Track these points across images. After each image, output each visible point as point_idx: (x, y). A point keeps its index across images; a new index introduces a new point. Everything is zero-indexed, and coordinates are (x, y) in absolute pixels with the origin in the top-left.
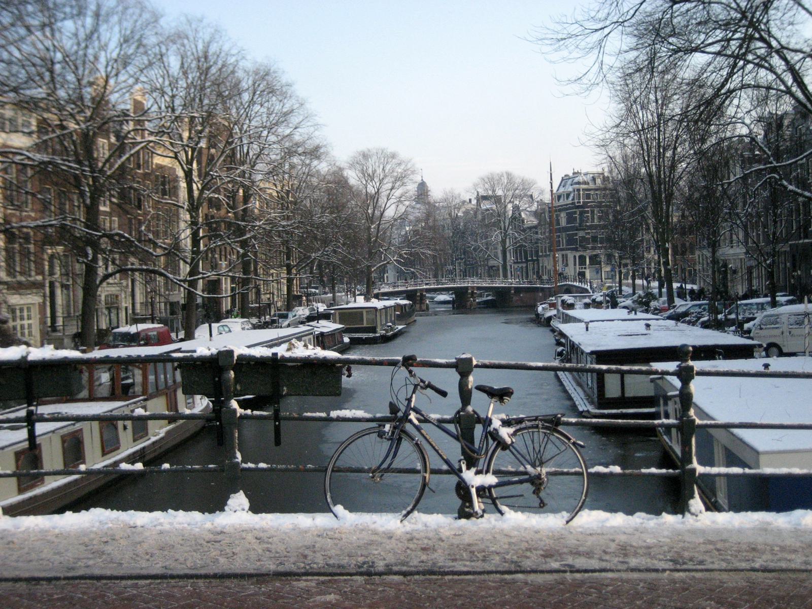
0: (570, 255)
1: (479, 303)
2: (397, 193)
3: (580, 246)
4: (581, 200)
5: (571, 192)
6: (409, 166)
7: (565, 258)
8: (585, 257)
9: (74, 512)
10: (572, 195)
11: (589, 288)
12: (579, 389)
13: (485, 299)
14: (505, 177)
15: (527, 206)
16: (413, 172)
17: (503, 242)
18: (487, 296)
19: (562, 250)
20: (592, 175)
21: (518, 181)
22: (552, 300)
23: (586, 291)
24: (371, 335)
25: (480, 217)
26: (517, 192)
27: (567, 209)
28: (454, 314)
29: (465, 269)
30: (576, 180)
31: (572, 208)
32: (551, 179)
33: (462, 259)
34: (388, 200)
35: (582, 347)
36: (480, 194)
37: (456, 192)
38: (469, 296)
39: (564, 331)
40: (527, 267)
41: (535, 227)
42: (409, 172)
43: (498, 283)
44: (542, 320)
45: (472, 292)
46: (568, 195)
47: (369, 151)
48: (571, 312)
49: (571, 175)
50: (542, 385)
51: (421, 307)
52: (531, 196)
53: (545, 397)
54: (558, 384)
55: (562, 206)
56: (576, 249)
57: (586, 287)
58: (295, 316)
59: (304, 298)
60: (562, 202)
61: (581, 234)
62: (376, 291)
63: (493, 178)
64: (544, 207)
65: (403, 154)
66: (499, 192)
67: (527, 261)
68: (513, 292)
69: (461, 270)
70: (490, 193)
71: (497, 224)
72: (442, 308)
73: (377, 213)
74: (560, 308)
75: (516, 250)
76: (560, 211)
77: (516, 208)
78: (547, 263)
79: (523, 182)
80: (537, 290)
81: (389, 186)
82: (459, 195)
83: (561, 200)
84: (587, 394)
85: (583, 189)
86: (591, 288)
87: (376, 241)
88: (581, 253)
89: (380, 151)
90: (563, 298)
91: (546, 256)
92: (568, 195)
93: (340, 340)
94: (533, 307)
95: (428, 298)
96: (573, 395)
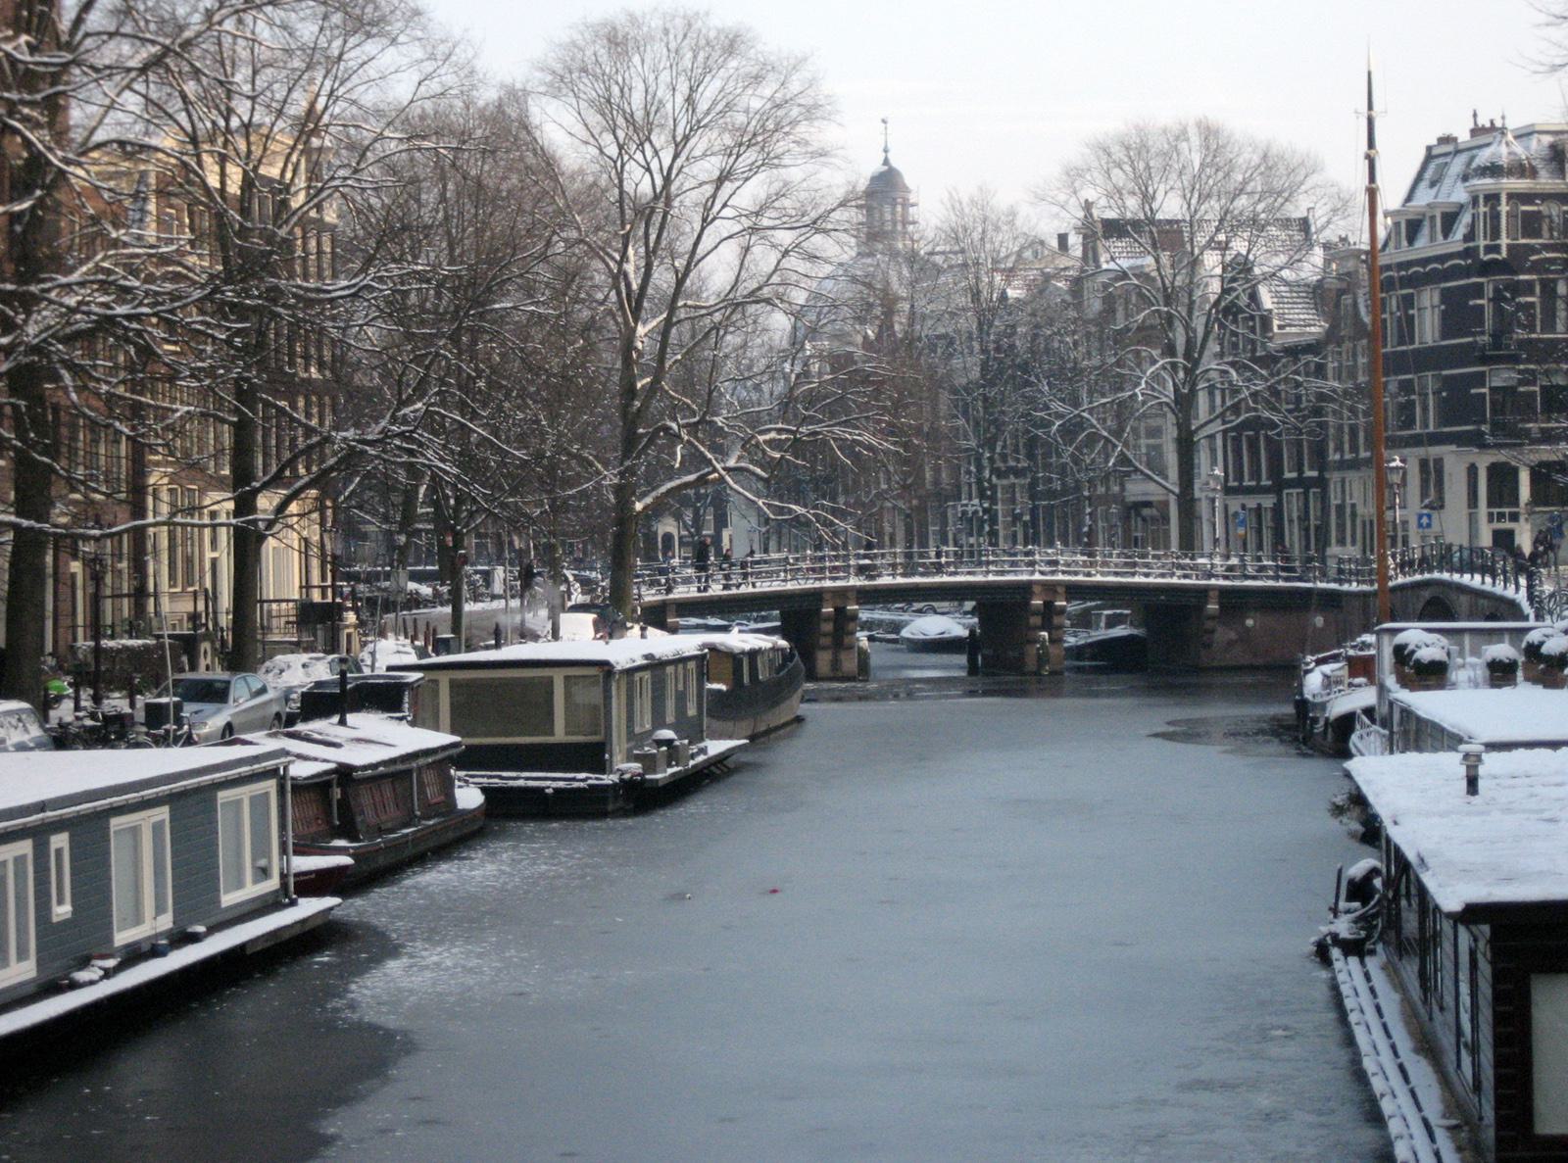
0: (1455, 462)
1: (1077, 652)
2: (749, 194)
3: (1496, 427)
4: (1504, 241)
5: (1462, 206)
6: (795, 86)
7: (1432, 475)
8: (1514, 473)
9: (1545, 687)
10: (1466, 219)
11: (1521, 597)
12: (1421, 1072)
13: (1102, 633)
14: (1195, 140)
15: (1281, 259)
16: (811, 112)
17: (1184, 403)
18: (1112, 622)
19: (1417, 441)
20: (1547, 139)
21: (1248, 157)
22: (1365, 646)
23: (1511, 609)
24: (583, 779)
25: (1095, 306)
26: (1242, 202)
27: (1448, 275)
28: (972, 693)
29: (1033, 511)
30: (1484, 157)
31: (1466, 272)
32: (1371, 144)
33: (1018, 473)
34: (706, 222)
35: (1429, 881)
36: (1096, 213)
37: (1001, 202)
38: (1035, 620)
39: (1382, 805)
40: (1277, 510)
41: (1314, 348)
42: (795, 112)
43: (1154, 573)
44: (1319, 727)
45: (1048, 605)
46: (1450, 220)
47: (633, 20)
48: (1426, 703)
49: (1464, 137)
50: (1264, 1034)
51: (836, 664)
52: (1304, 224)
53: (1264, 1101)
54: (1335, 1034)
55: (1424, 262)
56: (1476, 440)
57: (1510, 592)
58: (263, 690)
59: (351, 617)
60: (1425, 246)
61: (1502, 377)
62: (650, 596)
63: (1143, 147)
64: (1351, 265)
65: (773, 38)
66: (1170, 207)
67: (1279, 486)
68: (1213, 607)
69: (1016, 518)
70: (1132, 206)
71: (1155, 334)
72: (932, 669)
73: (663, 278)
74: (1390, 681)
75: (1237, 440)
76: (1416, 282)
77: (1240, 270)
78: (1355, 491)
79: (1268, 163)
80: (1300, 601)
81: (711, 167)
82: (1013, 214)
83: (1422, 241)
84: (1454, 1105)
85: (1511, 196)
86: (1531, 598)
87: (653, 388)
88: (1502, 456)
89: (679, 22)
90: (1400, 638)
91: (1354, 465)
92: (1450, 220)
93: (432, 793)
94: (1292, 672)
95: (868, 625)
96: (1387, 1106)
